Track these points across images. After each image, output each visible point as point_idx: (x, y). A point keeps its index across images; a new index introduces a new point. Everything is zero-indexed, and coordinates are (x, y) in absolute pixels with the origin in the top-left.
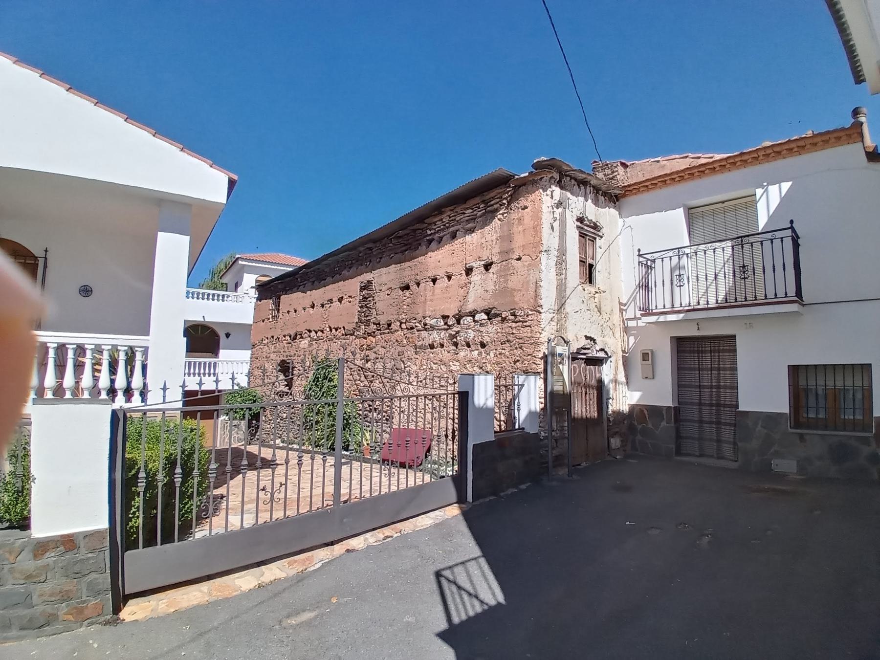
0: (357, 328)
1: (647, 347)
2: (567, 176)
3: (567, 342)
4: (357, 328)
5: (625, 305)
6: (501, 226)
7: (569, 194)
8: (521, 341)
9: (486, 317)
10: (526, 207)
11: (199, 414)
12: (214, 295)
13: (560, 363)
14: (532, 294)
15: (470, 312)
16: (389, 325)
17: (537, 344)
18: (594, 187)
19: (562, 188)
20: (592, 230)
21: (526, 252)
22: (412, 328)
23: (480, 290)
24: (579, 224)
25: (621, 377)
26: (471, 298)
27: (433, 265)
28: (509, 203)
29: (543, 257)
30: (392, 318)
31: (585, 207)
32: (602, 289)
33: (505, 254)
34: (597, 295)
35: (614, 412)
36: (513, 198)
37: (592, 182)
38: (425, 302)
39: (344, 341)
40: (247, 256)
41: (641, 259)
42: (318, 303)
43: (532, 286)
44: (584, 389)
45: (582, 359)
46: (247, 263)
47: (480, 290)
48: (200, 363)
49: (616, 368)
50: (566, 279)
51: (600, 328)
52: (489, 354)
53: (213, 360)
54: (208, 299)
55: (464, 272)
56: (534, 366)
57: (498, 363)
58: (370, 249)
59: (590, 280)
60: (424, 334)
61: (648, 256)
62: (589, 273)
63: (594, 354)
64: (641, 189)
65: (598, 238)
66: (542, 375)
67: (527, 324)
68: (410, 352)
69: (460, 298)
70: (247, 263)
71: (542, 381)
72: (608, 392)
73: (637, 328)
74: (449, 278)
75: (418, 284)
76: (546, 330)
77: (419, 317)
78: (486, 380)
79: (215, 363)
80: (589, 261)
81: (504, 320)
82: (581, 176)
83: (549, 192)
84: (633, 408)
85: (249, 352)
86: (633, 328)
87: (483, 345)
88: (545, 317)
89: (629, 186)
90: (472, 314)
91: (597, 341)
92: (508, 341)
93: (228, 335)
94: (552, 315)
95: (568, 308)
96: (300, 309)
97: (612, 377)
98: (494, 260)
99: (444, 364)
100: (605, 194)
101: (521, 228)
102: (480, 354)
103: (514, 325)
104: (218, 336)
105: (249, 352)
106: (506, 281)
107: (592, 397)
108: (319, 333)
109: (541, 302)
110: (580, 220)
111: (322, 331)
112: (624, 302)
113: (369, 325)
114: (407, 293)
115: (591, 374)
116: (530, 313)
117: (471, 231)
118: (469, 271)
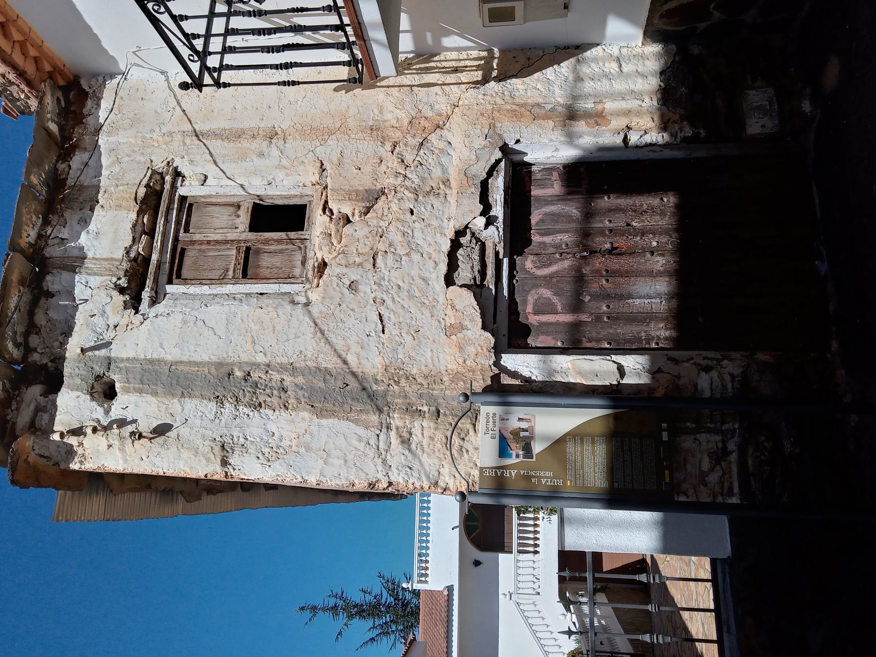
7: (73, 347)
13: (527, 450)
20: (158, 238)
24: (146, 295)
35: (664, 126)
44: (598, 262)
45: (512, 266)
48: (520, 531)
50: (292, 369)
61: (195, 67)
64: (17, 37)
65: (182, 191)
72: (603, 149)
83: (73, 440)
84: (651, 33)
91: (460, 225)
95: (371, 362)
97: (558, 135)
115: (554, 217)
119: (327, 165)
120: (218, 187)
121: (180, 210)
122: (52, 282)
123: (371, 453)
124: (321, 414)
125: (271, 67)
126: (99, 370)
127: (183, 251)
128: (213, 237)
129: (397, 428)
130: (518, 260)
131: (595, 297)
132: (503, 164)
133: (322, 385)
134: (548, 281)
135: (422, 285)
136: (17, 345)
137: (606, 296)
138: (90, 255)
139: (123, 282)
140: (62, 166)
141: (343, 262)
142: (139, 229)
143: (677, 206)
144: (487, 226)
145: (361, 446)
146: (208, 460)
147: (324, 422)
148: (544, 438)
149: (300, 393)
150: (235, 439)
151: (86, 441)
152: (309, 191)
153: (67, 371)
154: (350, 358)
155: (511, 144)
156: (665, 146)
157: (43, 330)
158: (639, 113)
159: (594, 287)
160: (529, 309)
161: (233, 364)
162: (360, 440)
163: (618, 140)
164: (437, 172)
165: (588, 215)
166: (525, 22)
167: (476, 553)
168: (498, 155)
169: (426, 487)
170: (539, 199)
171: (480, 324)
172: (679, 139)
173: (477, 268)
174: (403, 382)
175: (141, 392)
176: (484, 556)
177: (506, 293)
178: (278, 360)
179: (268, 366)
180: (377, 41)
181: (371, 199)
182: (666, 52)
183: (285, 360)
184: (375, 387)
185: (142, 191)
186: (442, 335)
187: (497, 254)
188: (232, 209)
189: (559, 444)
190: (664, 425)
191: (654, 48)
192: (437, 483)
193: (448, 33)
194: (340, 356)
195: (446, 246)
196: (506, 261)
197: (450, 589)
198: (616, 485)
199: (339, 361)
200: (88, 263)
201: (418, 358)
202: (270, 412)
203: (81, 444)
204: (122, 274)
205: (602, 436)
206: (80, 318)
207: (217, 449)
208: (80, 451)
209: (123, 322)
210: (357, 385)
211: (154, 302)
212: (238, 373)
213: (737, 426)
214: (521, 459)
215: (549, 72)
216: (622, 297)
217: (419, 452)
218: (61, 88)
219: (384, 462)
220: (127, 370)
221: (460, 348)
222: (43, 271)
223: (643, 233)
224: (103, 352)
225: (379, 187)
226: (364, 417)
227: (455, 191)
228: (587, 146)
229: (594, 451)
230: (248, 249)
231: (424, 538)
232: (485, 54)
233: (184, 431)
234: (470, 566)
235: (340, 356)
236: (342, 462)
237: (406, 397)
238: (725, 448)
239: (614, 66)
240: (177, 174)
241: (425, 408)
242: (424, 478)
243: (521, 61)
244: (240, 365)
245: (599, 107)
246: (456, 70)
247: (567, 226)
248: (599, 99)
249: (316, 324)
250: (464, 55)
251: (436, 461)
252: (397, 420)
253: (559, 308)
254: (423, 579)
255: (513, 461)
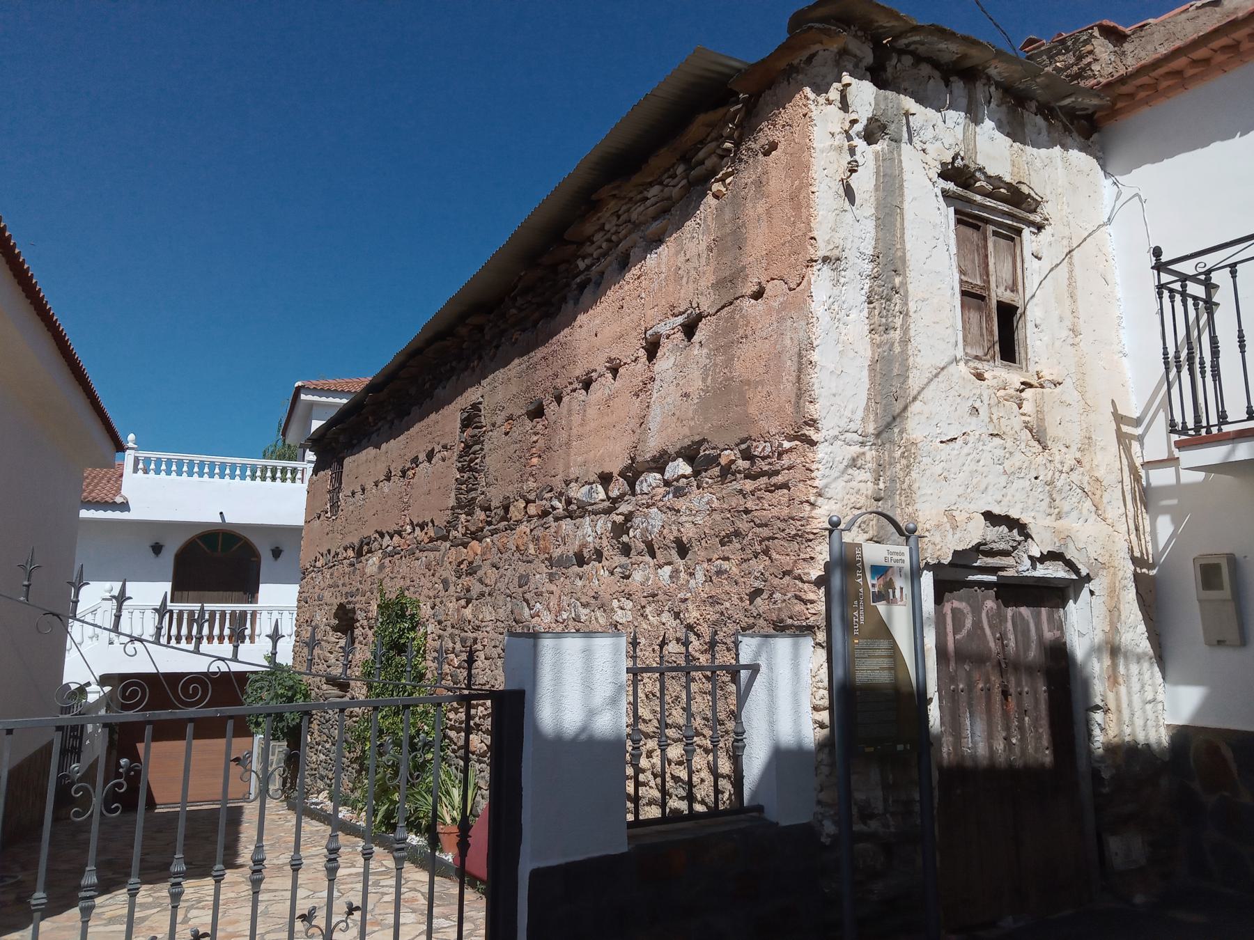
0: (451, 525)
1: (1214, 545)
2: (902, 52)
3: (908, 534)
4: (451, 525)
5: (1137, 422)
6: (720, 210)
7: (909, 103)
8: (765, 532)
9: (688, 470)
10: (773, 146)
11: (230, 724)
12: (284, 470)
13: (879, 597)
14: (788, 387)
15: (654, 459)
16: (506, 509)
17: (802, 537)
18: (998, 85)
19: (880, 83)
21: (774, 271)
22: (545, 514)
23: (672, 396)
24: (950, 186)
25: (1135, 634)
26: (655, 421)
27: (584, 346)
28: (738, 145)
29: (820, 282)
30: (510, 491)
31: (969, 140)
32: (1047, 375)
33: (728, 282)
34: (1028, 393)
35: (1111, 749)
36: (748, 127)
37: (992, 71)
38: (568, 444)
39: (431, 555)
40: (320, 383)
41: (1166, 278)
42: (396, 470)
43: (790, 365)
44: (995, 680)
45: (987, 585)
46: (316, 398)
47: (674, 396)
49: (1114, 612)
50: (905, 341)
51: (1040, 490)
52: (692, 575)
53: (248, 607)
54: (293, 480)
55: (642, 353)
56: (799, 607)
57: (714, 601)
58: (481, 328)
59: (1008, 350)
60: (566, 525)
61: (1187, 268)
62: (1003, 332)
63: (1020, 567)
65: (1026, 232)
66: (821, 636)
67: (779, 479)
68: (540, 578)
69: (633, 423)
70: (316, 398)
71: (822, 654)
72: (1086, 685)
73: (1178, 489)
74: (614, 371)
75: (559, 399)
76: (835, 487)
77: (558, 483)
78: (588, 653)
79: (254, 614)
80: (999, 293)
81: (727, 472)
82: (949, 50)
83: (834, 94)
84: (1182, 735)
85: (295, 588)
86: (1166, 491)
87: (683, 549)
88: (828, 456)
89: (1123, 80)
90: (659, 463)
91: (1033, 530)
92: (737, 533)
93: (277, 553)
94: (856, 449)
95: (917, 426)
96: (369, 485)
97: (1098, 637)
98: (705, 307)
99: (602, 607)
100: (1047, 111)
101: (761, 207)
102: (675, 575)
103: (749, 485)
104: (258, 556)
105: (295, 588)
106: (728, 363)
107: (1027, 703)
108: (396, 538)
109: (814, 411)
110: (948, 173)
111: (399, 533)
112: (1135, 414)
113: (475, 514)
114: (540, 424)
116: (787, 445)
117: (658, 241)
118: (652, 349)
119: (1060, 388)
120: (1034, 271)
121: (1010, 227)
122: (958, 85)
123: (843, 423)
124: (872, 368)
125: (1164, 343)
126: (892, 128)
127: (977, 228)
128: (991, 261)
129: (864, 454)
130: (992, 593)
131: (969, 674)
132: (1074, 577)
133: (895, 372)
134: (977, 624)
135: (983, 487)
136: (908, 45)
137: (971, 686)
138: (978, 129)
139: (959, 163)
140: (1033, 105)
141: (992, 402)
142: (997, 183)
143: (1043, 765)
144: (1031, 558)
145: (848, 413)
146: (828, 242)
147: (866, 373)
148: (889, 614)
149: (886, 348)
150: (843, 273)
151: (834, 110)
152: (1033, 368)
153: (889, 93)
154: (917, 403)
155: (1091, 586)
156: (1090, 752)
157: (916, 71)
158: (1120, 722)
159: (976, 675)
160: (956, 604)
161: (905, 277)
162: (853, 412)
163: (1098, 701)
164: (1066, 506)
165: (1030, 669)
166: (1200, 601)
167: (172, 548)
168: (1084, 572)
169: (816, 483)
170: (1039, 614)
171: (959, 548)
172: (1096, 765)
173: (995, 546)
174: (904, 462)
175: (877, 173)
176: (168, 559)
177: (971, 578)
178: (912, 326)
179: (907, 314)
180: (1232, 451)
181: (1039, 437)
182: (1163, 750)
183: (912, 333)
184: (896, 430)
185: (1025, 189)
186: (945, 507)
187: (1002, 569)
188: (1010, 283)
189: (883, 631)
190: (908, 747)
191: (1165, 740)
192: (820, 495)
193: (1176, 522)
194: (919, 393)
195: (1014, 514)
196: (993, 578)
197: (124, 507)
198: (858, 693)
199: (915, 392)
200: (972, 126)
201: (924, 479)
202: (865, 313)
203: (829, 102)
204: (966, 162)
205: (896, 678)
206: (930, 112)
207: (836, 253)
208: (821, 99)
209: (928, 159)
210: (897, 411)
211: (946, 195)
212: (897, 280)
213: (892, 830)
214: (872, 590)
215: (1142, 628)
216: (970, 706)
217: (846, 477)
218: (1094, 113)
219: (836, 438)
220: (892, 159)
221: (938, 526)
222: (952, 75)
223: (1021, 728)
224: (905, 135)
225: (1049, 443)
226: (872, 417)
227: (1054, 524)
228: (1089, 669)
229: (882, 669)
230: (982, 298)
231: (206, 470)
232: (1151, 561)
233: (849, 217)
234: (154, 537)
235: (919, 393)
236: (834, 391)
237: (890, 464)
238: (872, 816)
239: (1150, 697)
240: (1040, 228)
241: (882, 486)
242: (825, 481)
243: (1151, 594)
244: (904, 284)
245: (1121, 680)
246: (1137, 529)
247: (1021, 646)
248: (1128, 676)
249: (943, 369)
250: (1148, 538)
251: (839, 497)
252: (870, 454)
253: (958, 637)
254: (141, 466)
255: (870, 581)
